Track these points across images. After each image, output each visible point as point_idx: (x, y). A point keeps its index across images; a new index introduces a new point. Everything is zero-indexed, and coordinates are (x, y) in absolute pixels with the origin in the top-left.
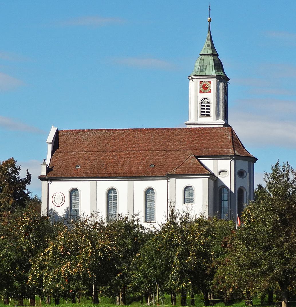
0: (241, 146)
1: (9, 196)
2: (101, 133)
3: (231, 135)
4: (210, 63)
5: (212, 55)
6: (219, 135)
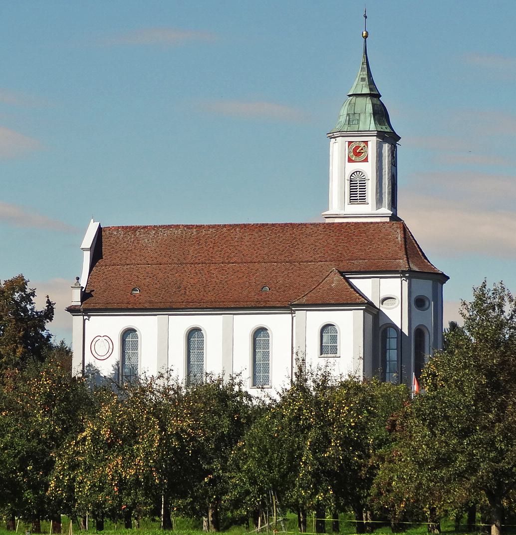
0: (421, 254)
1: (15, 342)
2: (176, 232)
3: (403, 236)
4: (367, 109)
5: (370, 95)
6: (382, 235)
